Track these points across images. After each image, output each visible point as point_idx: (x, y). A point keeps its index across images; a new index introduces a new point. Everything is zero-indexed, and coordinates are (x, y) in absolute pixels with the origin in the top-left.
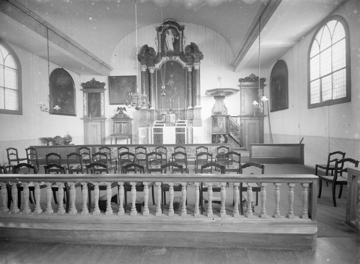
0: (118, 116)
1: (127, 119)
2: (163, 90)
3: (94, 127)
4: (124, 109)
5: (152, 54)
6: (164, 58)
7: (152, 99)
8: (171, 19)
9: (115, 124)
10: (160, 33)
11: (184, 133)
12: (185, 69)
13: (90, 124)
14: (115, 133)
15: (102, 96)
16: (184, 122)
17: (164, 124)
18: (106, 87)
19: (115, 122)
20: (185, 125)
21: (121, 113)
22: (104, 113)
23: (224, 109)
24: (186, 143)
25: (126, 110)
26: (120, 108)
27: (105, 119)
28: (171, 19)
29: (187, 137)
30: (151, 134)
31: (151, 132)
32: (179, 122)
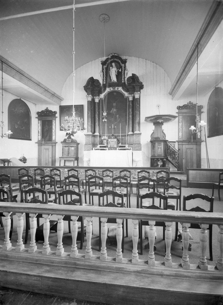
8: (114, 54)
10: (105, 67)
13: (43, 147)
15: (54, 123)
16: (125, 147)
18: (58, 115)
22: (55, 138)
27: (56, 144)
28: (114, 54)
32: (120, 147)
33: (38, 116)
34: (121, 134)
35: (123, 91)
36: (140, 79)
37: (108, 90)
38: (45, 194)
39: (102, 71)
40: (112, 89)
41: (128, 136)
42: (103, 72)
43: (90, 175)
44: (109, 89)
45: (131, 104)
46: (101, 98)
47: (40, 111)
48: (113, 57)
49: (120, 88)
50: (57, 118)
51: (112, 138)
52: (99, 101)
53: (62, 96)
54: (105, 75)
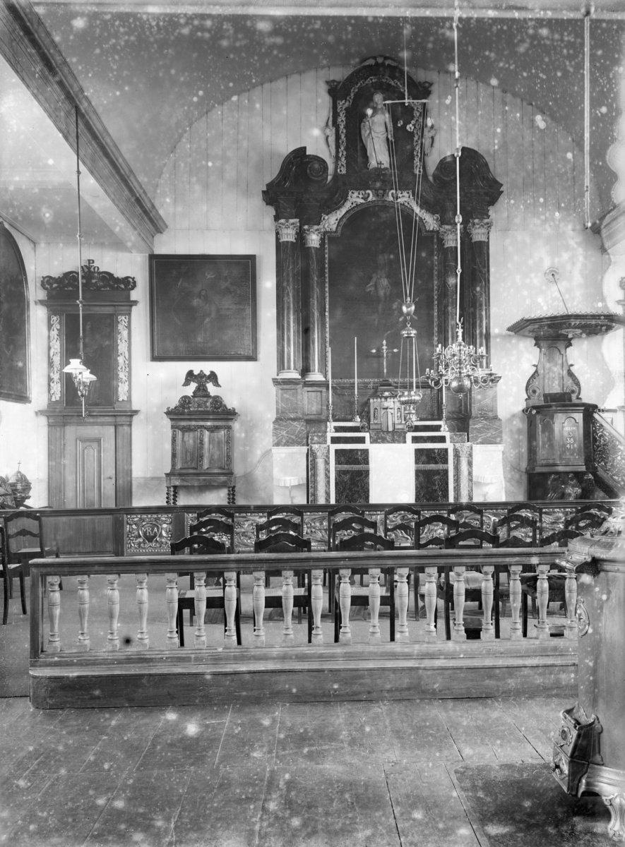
0: (189, 403)
1: (225, 417)
2: (408, 318)
3: (88, 444)
4: (213, 377)
5: (320, 179)
6: (356, 194)
7: (314, 343)
8: (386, 58)
9: (180, 434)
10: (343, 105)
11: (444, 466)
12: (432, 237)
13: (71, 431)
14: (179, 466)
15: (121, 327)
16: (437, 428)
17: (367, 435)
18: (140, 294)
19: (177, 427)
20: (442, 439)
21: (201, 391)
22: (130, 391)
23: (569, 382)
24: (451, 500)
25: (217, 384)
26: (196, 373)
27: (131, 416)
28: (386, 58)
29: (457, 480)
30: (327, 471)
31: (327, 463)
32: (417, 429)
33: (50, 296)
34: (358, 378)
35: (343, 210)
36: (268, 179)
37: (355, 198)
39: (330, 123)
40: (371, 198)
41: (319, 394)
42: (335, 124)
43: (465, 525)
44: (361, 196)
46: (328, 229)
47: (56, 272)
48: (364, 72)
49: (405, 194)
50: (134, 308)
51: (387, 394)
52: (322, 240)
53: (165, 207)
54: (343, 136)
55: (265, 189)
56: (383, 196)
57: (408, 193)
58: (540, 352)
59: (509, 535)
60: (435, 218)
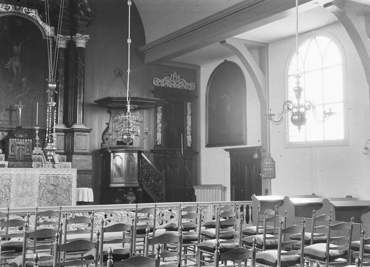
38: (189, 144)
45: (62, 58)
49: (33, 11)
55: (230, 156)
56: (19, 10)
57: (35, 11)
58: (111, 116)
59: (36, 228)
60: (52, 29)
